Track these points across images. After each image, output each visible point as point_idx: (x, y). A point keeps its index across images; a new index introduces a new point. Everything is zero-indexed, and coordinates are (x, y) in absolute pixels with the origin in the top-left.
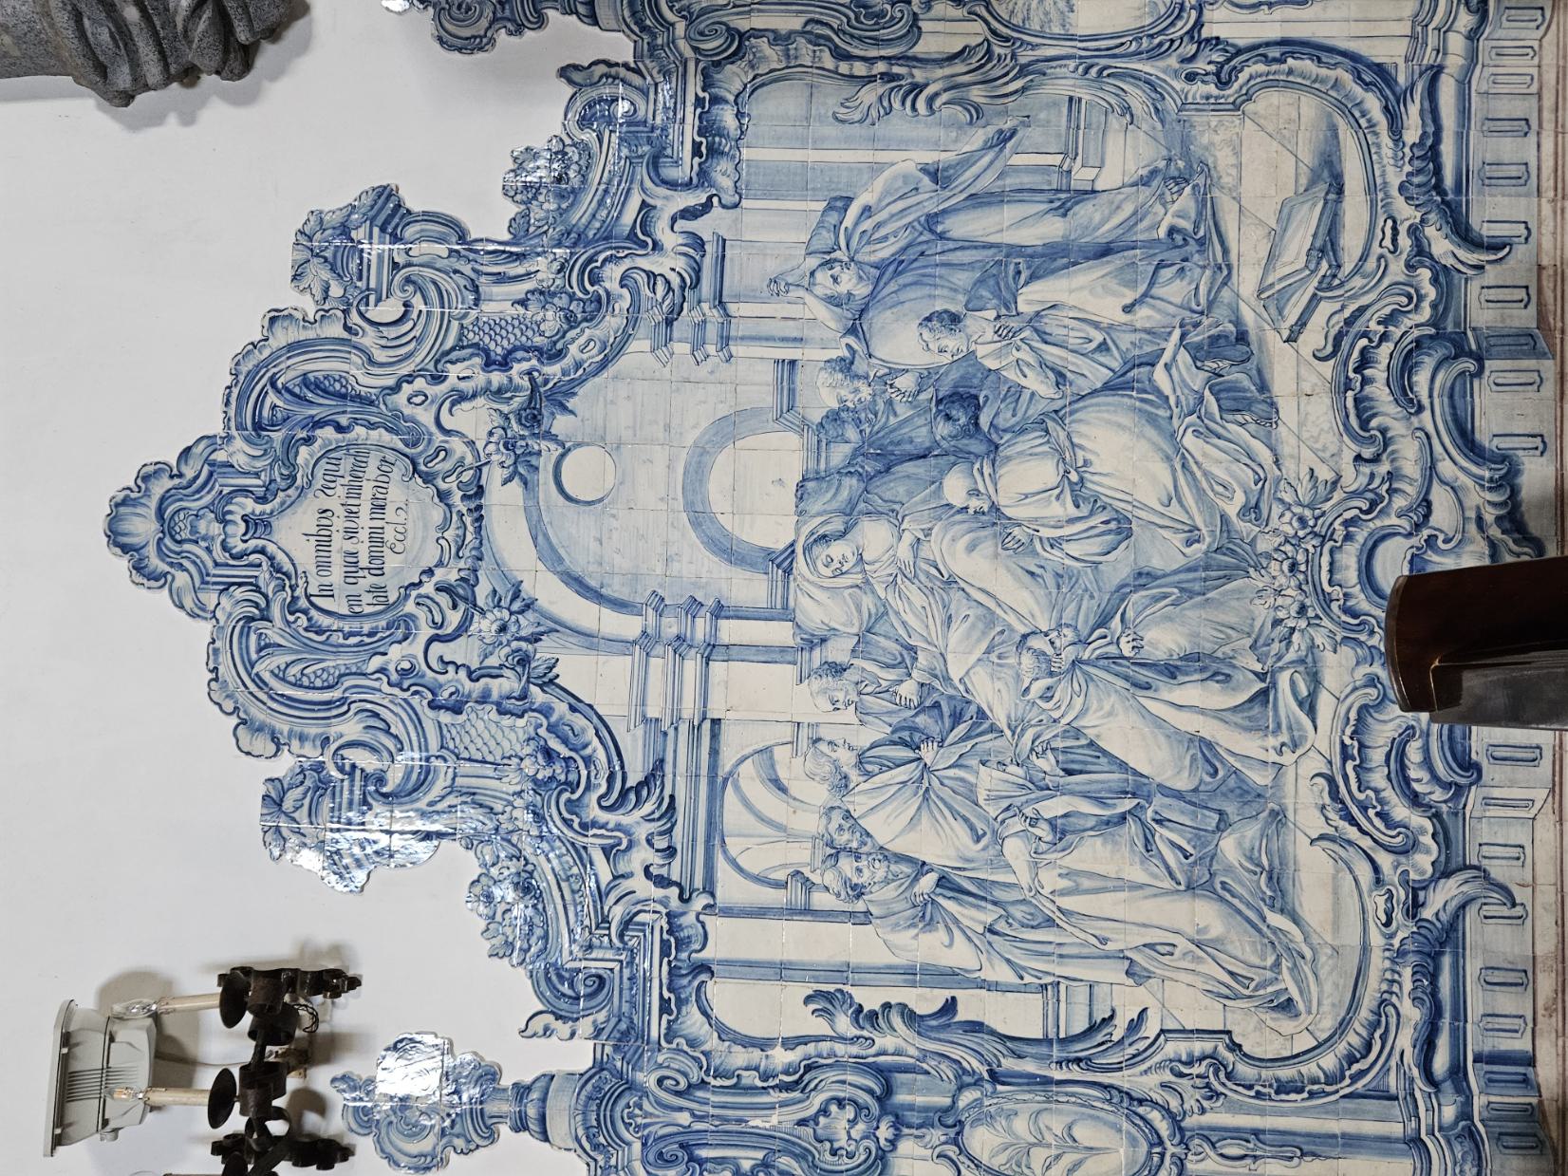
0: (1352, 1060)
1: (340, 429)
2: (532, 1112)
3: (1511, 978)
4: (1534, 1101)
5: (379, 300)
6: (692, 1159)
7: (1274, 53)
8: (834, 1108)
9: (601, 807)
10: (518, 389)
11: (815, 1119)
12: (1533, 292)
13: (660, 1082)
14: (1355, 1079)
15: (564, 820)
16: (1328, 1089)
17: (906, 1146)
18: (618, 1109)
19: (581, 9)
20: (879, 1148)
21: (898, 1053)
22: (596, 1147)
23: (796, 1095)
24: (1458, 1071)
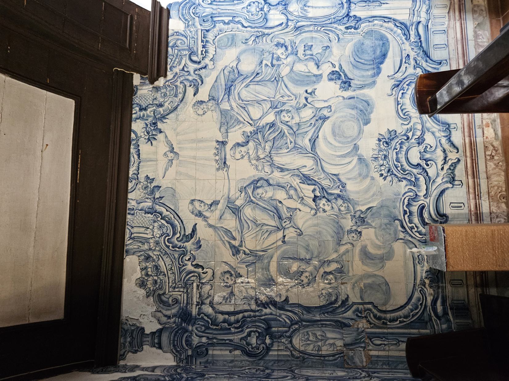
0: (412, 310)
2: (156, 341)
3: (439, 46)
4: (470, 321)
6: (213, 21)
7: (371, 20)
8: (252, 4)
9: (178, 241)
10: (150, 117)
11: (246, 337)
12: (448, 61)
14: (413, 316)
15: (166, 246)
16: (405, 320)
17: (271, 12)
18: (191, 11)
19: (157, 346)
20: (267, 346)
21: (271, 314)
22: (177, 351)
23: (240, 329)
24: (445, 313)
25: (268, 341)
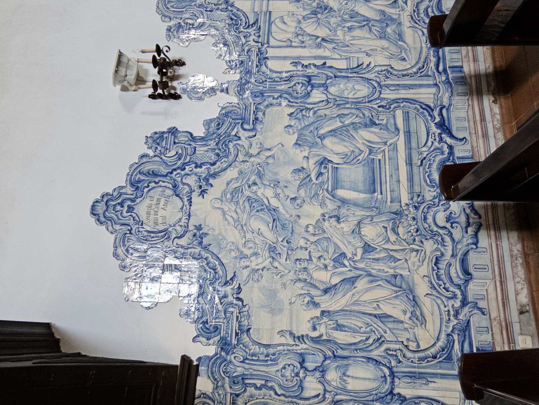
1: (156, 183)
5: (170, 151)
13: (235, 358)
25: (309, 88)
